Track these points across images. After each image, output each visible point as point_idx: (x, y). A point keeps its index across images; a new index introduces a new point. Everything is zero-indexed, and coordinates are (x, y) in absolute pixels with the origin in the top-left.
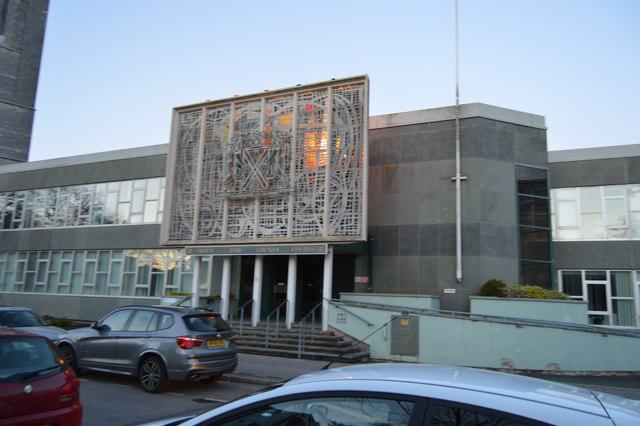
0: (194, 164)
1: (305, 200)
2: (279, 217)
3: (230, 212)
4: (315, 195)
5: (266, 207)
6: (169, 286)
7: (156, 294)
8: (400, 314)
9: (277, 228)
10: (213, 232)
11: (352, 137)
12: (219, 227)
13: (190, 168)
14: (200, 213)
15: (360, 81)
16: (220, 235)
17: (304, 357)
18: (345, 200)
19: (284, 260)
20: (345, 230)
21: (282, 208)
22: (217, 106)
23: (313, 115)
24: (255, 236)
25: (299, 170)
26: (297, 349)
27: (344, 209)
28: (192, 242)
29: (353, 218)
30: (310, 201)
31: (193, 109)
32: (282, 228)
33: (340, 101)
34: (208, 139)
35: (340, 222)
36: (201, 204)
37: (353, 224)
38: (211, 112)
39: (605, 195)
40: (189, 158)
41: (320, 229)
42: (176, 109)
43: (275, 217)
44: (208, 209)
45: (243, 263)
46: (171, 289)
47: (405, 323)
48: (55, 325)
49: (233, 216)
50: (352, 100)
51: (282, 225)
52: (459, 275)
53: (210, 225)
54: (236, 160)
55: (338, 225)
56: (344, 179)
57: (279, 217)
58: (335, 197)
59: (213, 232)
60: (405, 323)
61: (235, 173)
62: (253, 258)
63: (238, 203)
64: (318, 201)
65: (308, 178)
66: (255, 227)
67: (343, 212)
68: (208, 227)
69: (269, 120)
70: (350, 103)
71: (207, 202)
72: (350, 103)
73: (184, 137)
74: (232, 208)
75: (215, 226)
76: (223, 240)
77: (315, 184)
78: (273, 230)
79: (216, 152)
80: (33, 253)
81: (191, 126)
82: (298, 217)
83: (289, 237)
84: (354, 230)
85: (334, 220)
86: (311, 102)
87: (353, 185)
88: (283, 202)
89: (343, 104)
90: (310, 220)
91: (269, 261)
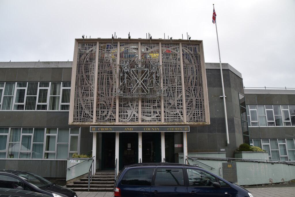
0: (90, 74)
1: (171, 101)
2: (155, 110)
3: (120, 105)
4: (176, 99)
5: (145, 104)
6: (47, 152)
7: (14, 157)
8: (227, 162)
9: (154, 116)
10: (108, 117)
11: (195, 70)
12: (113, 115)
13: (88, 77)
14: (98, 105)
15: (199, 43)
16: (115, 120)
17: (91, 190)
18: (194, 103)
19: (136, 136)
20: (196, 119)
21: (156, 105)
22: (114, 42)
23: (171, 55)
24: (140, 120)
25: (165, 84)
26: (87, 183)
27: (194, 108)
28: (94, 123)
29: (200, 113)
30: (174, 102)
31: (92, 42)
32: (157, 116)
33: (187, 51)
34: (101, 60)
35: (192, 115)
36: (98, 100)
37: (200, 116)
38: (102, 45)
39: (35, 109)
40: (87, 70)
41: (181, 118)
42: (78, 41)
43: (152, 110)
44: (104, 103)
45: (103, 137)
46: (72, 154)
47: (230, 166)
48: (268, 184)
49: (122, 108)
50: (193, 51)
51: (157, 115)
52: (228, 142)
53: (105, 113)
54: (126, 75)
55: (192, 116)
56: (193, 92)
57: (155, 110)
58: (189, 100)
59: (108, 117)
60: (230, 166)
61: (126, 82)
62: (114, 134)
63: (125, 102)
64: (179, 102)
65: (171, 89)
66: (140, 116)
67: (194, 110)
68: (104, 114)
69: (144, 55)
70: (192, 53)
71: (103, 99)
72: (192, 53)
73: (83, 57)
74: (121, 103)
75: (109, 114)
76: (117, 123)
77: (176, 93)
78: (152, 117)
79: (107, 69)
80: (40, 129)
81: (88, 51)
82: (167, 110)
83: (163, 122)
84: (201, 119)
85: (189, 114)
86: (170, 49)
87: (198, 95)
88: (157, 102)
89: (189, 53)
90: (175, 113)
91: (123, 136)
